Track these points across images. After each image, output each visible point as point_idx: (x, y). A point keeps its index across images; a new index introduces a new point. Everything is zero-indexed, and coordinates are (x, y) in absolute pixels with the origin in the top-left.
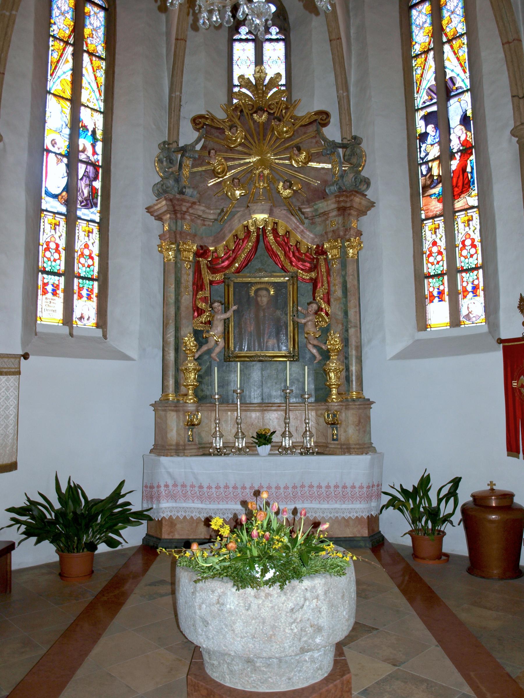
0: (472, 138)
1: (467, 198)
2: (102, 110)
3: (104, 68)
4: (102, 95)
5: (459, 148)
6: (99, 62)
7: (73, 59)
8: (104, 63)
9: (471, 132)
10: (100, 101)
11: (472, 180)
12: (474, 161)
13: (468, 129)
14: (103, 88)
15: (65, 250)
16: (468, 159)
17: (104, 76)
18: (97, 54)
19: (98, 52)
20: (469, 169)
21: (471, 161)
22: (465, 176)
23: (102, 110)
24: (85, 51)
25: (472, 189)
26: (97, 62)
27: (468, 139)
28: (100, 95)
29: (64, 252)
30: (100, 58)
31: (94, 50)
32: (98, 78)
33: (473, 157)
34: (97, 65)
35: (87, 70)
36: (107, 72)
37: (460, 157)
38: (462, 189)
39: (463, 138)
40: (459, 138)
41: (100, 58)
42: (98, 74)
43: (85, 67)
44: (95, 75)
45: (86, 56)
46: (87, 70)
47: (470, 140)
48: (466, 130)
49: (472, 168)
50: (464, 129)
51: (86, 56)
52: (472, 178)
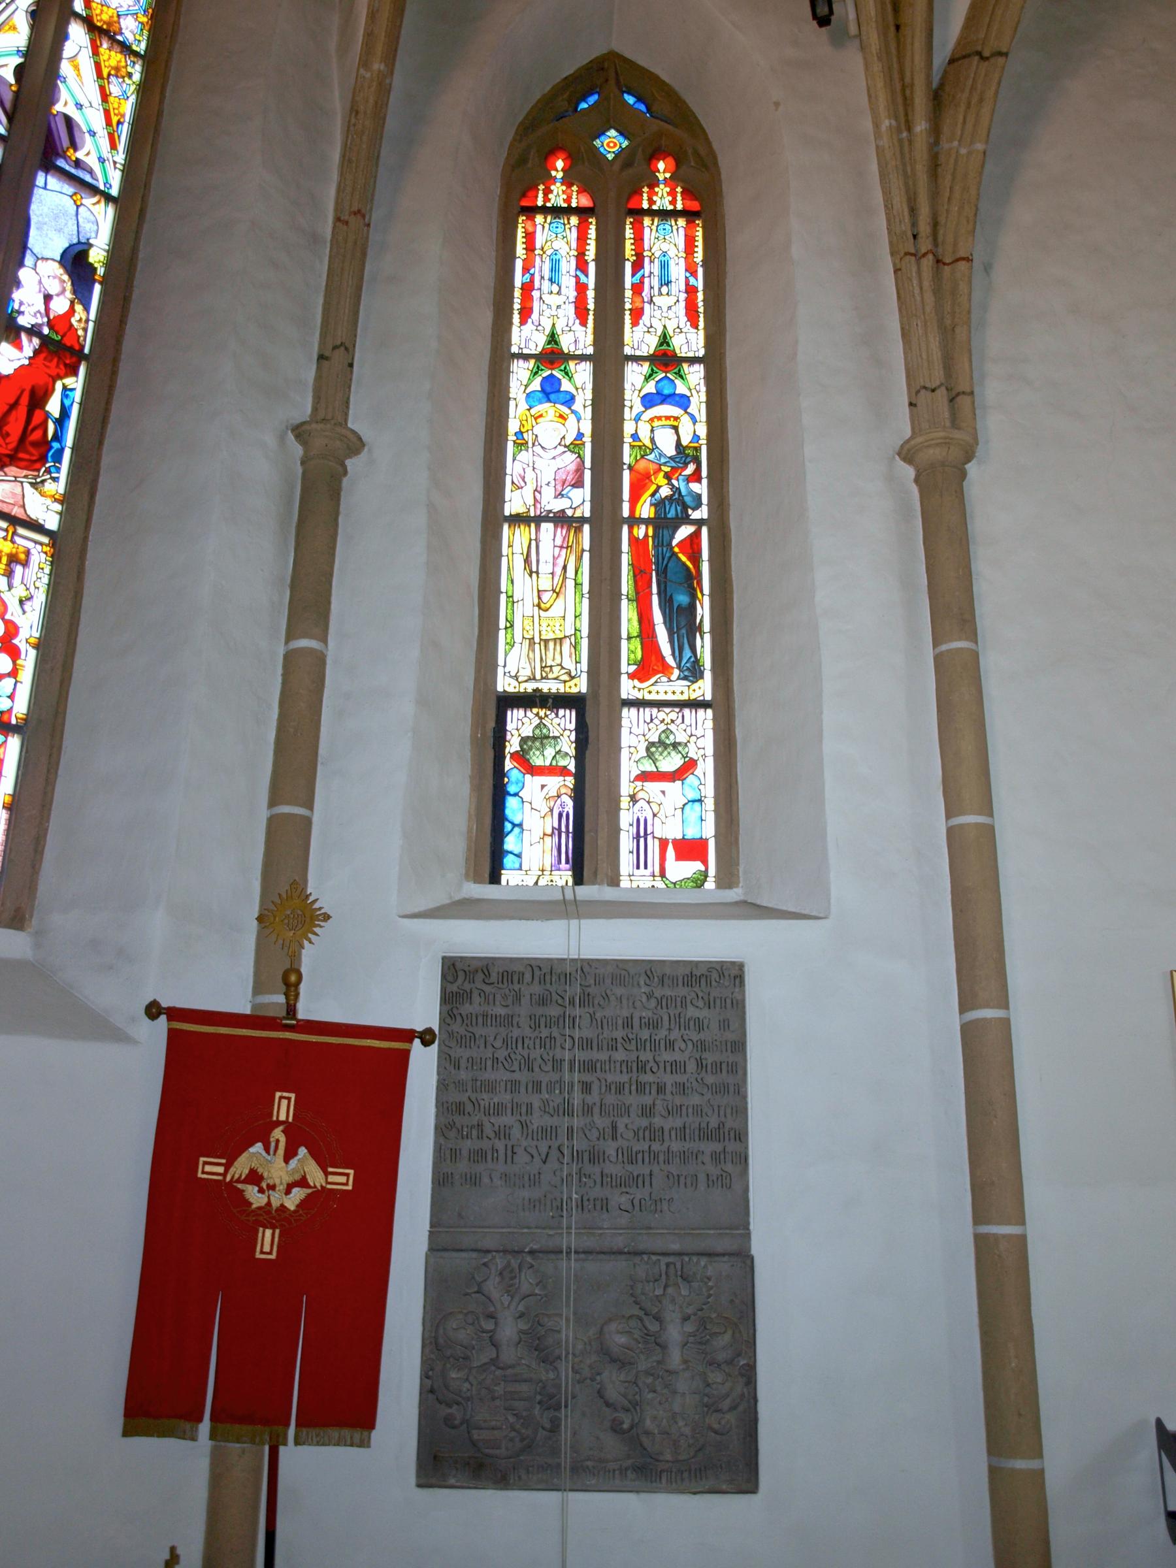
0: (85, 330)
1: (27, 486)
2: (114, 192)
3: (137, 77)
4: (122, 146)
5: (41, 325)
6: (119, 56)
7: (33, 27)
8: (138, 67)
9: (87, 309)
10: (109, 166)
11: (56, 445)
12: (77, 396)
13: (81, 291)
14: (125, 129)
15: (37, 647)
16: (61, 378)
17: (133, 99)
18: (119, 38)
19: (121, 34)
20: (53, 406)
21: (65, 388)
22: (37, 419)
23: (114, 192)
24: (77, 16)
25: (48, 471)
26: (112, 57)
27: (74, 321)
28: (113, 146)
29: (33, 653)
30: (125, 48)
31: (109, 24)
32: (111, 99)
33: (76, 383)
34: (113, 63)
35: (77, 68)
36: (144, 89)
37: (36, 352)
38: (17, 450)
39: (60, 306)
40: (48, 298)
41: (125, 48)
42: (114, 89)
43: (72, 59)
44: (102, 89)
45: (77, 33)
46: (77, 68)
47: (80, 333)
48: (74, 292)
49: (65, 412)
50: (68, 286)
51: (77, 33)
52: (57, 437)
